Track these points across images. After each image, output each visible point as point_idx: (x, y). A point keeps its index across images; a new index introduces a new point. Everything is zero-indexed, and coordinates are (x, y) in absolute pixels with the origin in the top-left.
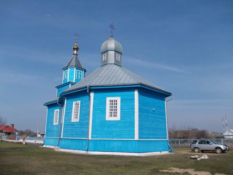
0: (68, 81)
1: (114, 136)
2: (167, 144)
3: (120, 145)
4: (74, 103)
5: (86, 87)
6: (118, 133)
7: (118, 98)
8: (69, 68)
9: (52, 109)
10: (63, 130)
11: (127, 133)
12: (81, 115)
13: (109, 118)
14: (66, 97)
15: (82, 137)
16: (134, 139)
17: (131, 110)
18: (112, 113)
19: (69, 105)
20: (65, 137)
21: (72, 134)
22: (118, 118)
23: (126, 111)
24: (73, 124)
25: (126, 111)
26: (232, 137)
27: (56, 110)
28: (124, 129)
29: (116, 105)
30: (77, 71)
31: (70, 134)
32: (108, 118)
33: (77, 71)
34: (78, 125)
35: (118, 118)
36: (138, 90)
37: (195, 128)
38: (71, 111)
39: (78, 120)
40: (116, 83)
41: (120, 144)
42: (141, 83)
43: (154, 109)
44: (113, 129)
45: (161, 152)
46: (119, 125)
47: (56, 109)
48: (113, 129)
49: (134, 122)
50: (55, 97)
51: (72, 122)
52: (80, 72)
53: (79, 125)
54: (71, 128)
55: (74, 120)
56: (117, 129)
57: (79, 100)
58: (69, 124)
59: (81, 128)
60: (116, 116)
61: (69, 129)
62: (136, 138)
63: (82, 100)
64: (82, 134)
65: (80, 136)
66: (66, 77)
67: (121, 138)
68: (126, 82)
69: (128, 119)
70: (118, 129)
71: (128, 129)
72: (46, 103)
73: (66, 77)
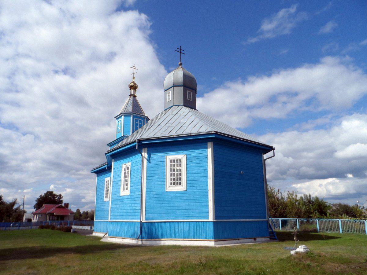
0: (122, 135)
1: (177, 215)
2: (210, 229)
3: (187, 229)
4: (124, 166)
5: (135, 142)
6: (184, 211)
7: (183, 156)
8: (123, 117)
9: (102, 177)
10: (111, 208)
11: (197, 211)
12: (132, 185)
13: (184, 187)
14: (113, 158)
15: (133, 219)
16: (209, 219)
17: (202, 175)
18: (174, 180)
19: (116, 170)
20: (114, 219)
21: (121, 214)
22: (183, 187)
23: (194, 175)
24: (122, 199)
25: (194, 175)
26: (2, 228)
27: (107, 179)
28: (192, 204)
29: (180, 168)
30: (135, 119)
31: (118, 214)
32: (169, 188)
33: (135, 119)
34: (128, 200)
35: (183, 187)
36: (212, 143)
37: (38, 197)
38: (119, 179)
39: (127, 193)
40: (180, 133)
41: (186, 227)
42: (216, 132)
43: (242, 172)
44: (176, 204)
45: (255, 239)
46: (185, 198)
47: (107, 177)
48: (176, 204)
49: (207, 192)
50: (100, 161)
51: (121, 195)
52: (139, 120)
53: (130, 200)
54: (121, 205)
55: (124, 193)
56: (182, 205)
57: (129, 162)
58: (118, 199)
59: (133, 205)
60: (180, 184)
61: (118, 206)
62: (211, 218)
63: (133, 161)
64: (133, 214)
65: (131, 217)
66: (120, 129)
67: (188, 218)
68: (195, 131)
69: (198, 188)
70: (184, 204)
71: (199, 203)
72: (94, 169)
73: (119, 128)
